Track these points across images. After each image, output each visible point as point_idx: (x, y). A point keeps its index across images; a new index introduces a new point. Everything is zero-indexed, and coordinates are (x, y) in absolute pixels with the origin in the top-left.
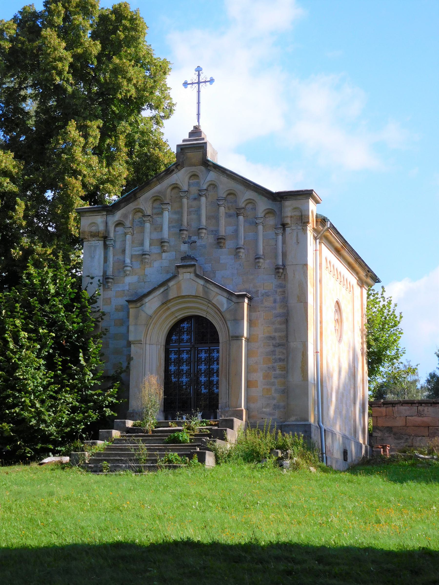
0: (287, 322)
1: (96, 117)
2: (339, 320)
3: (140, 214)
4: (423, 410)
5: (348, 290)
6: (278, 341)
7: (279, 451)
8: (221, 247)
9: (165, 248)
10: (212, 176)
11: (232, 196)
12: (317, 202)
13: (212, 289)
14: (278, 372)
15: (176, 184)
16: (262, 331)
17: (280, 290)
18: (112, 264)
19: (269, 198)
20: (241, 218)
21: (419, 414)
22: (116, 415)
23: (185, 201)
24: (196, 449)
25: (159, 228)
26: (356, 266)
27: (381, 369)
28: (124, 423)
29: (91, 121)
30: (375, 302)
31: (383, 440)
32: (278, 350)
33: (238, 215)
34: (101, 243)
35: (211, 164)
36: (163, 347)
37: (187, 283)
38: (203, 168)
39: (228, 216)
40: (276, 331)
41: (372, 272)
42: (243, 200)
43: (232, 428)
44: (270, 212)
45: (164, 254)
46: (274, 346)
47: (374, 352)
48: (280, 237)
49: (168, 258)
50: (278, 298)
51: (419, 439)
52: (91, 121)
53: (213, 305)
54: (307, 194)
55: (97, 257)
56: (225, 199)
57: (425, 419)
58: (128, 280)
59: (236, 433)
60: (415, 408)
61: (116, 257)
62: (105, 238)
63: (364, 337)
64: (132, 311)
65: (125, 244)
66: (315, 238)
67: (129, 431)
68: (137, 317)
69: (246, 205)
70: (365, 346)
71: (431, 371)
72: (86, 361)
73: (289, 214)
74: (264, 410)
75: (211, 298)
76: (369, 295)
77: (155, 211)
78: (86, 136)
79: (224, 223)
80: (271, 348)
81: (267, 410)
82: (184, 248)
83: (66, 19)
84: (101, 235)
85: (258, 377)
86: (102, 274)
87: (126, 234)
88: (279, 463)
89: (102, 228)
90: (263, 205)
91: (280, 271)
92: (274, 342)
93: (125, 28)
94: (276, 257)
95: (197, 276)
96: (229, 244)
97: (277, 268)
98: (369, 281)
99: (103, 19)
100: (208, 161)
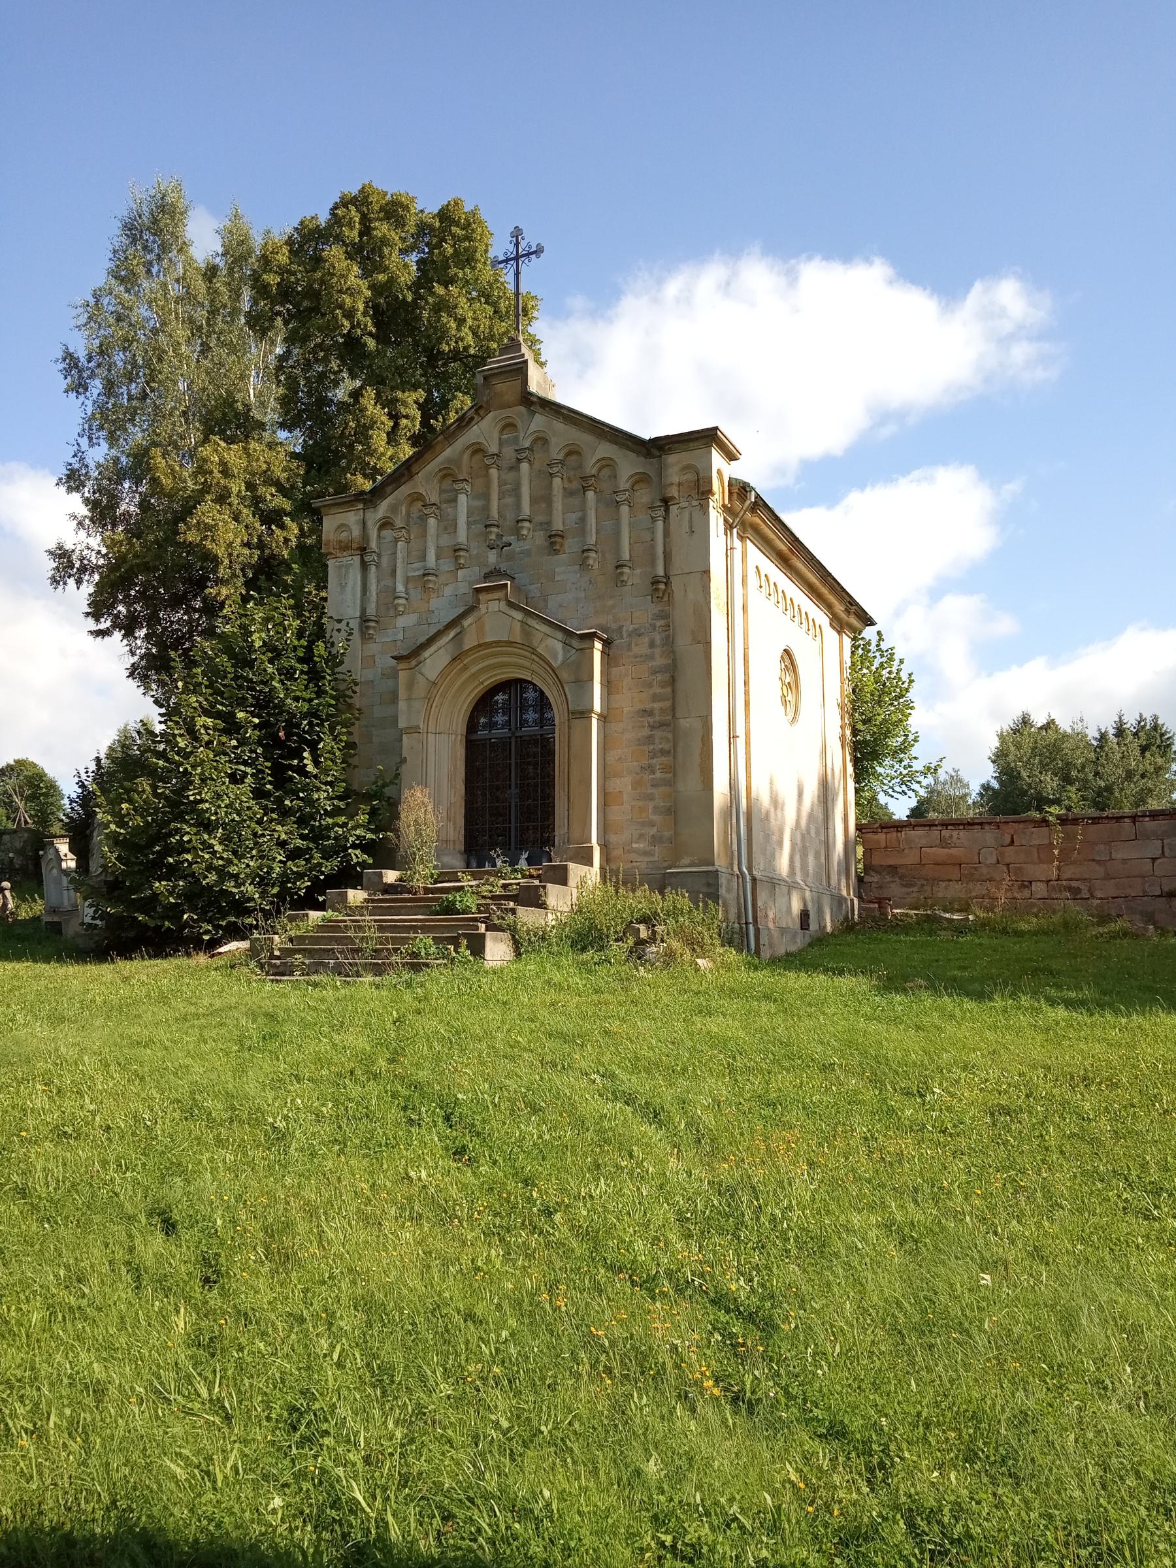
0: (673, 681)
1: (415, 387)
2: (793, 685)
3: (420, 504)
4: (951, 837)
5: (812, 632)
6: (657, 718)
7: (642, 927)
8: (557, 552)
9: (462, 561)
10: (539, 421)
11: (574, 457)
12: (731, 456)
13: (537, 627)
14: (658, 775)
15: (479, 443)
16: (628, 702)
17: (662, 622)
18: (374, 594)
19: (638, 453)
20: (590, 494)
21: (944, 843)
22: (371, 861)
23: (494, 472)
24: (477, 928)
25: (450, 526)
26: (824, 591)
27: (880, 770)
28: (380, 875)
29: (404, 392)
30: (865, 659)
31: (881, 887)
32: (658, 734)
33: (585, 489)
34: (357, 559)
35: (535, 399)
36: (459, 737)
37: (496, 621)
38: (522, 409)
39: (568, 493)
40: (655, 698)
41: (857, 604)
42: (594, 461)
43: (563, 881)
44: (641, 479)
45: (460, 572)
46: (652, 727)
47: (865, 742)
48: (660, 524)
49: (469, 577)
50: (658, 638)
51: (943, 884)
52: (404, 392)
53: (540, 656)
54: (709, 438)
55: (350, 585)
56: (562, 463)
57: (953, 851)
58: (401, 622)
59: (574, 891)
60: (935, 833)
61: (383, 583)
62: (363, 550)
63: (847, 716)
64: (403, 676)
65: (395, 560)
66: (729, 527)
67: (389, 889)
68: (410, 686)
69: (600, 470)
70: (848, 732)
71: (984, 781)
72: (316, 763)
73: (676, 479)
74: (635, 845)
75: (535, 643)
76: (855, 648)
77: (446, 496)
78: (395, 417)
79: (560, 508)
80: (646, 732)
81: (641, 846)
82: (492, 557)
83: (366, 231)
84: (355, 546)
85: (623, 785)
86: (358, 614)
87: (396, 540)
88: (638, 952)
89: (356, 532)
90: (628, 466)
91: (660, 587)
92: (651, 720)
93: (457, 239)
94: (653, 563)
95: (511, 605)
96: (571, 545)
97: (655, 582)
98: (854, 621)
99: (423, 228)
100: (531, 394)
